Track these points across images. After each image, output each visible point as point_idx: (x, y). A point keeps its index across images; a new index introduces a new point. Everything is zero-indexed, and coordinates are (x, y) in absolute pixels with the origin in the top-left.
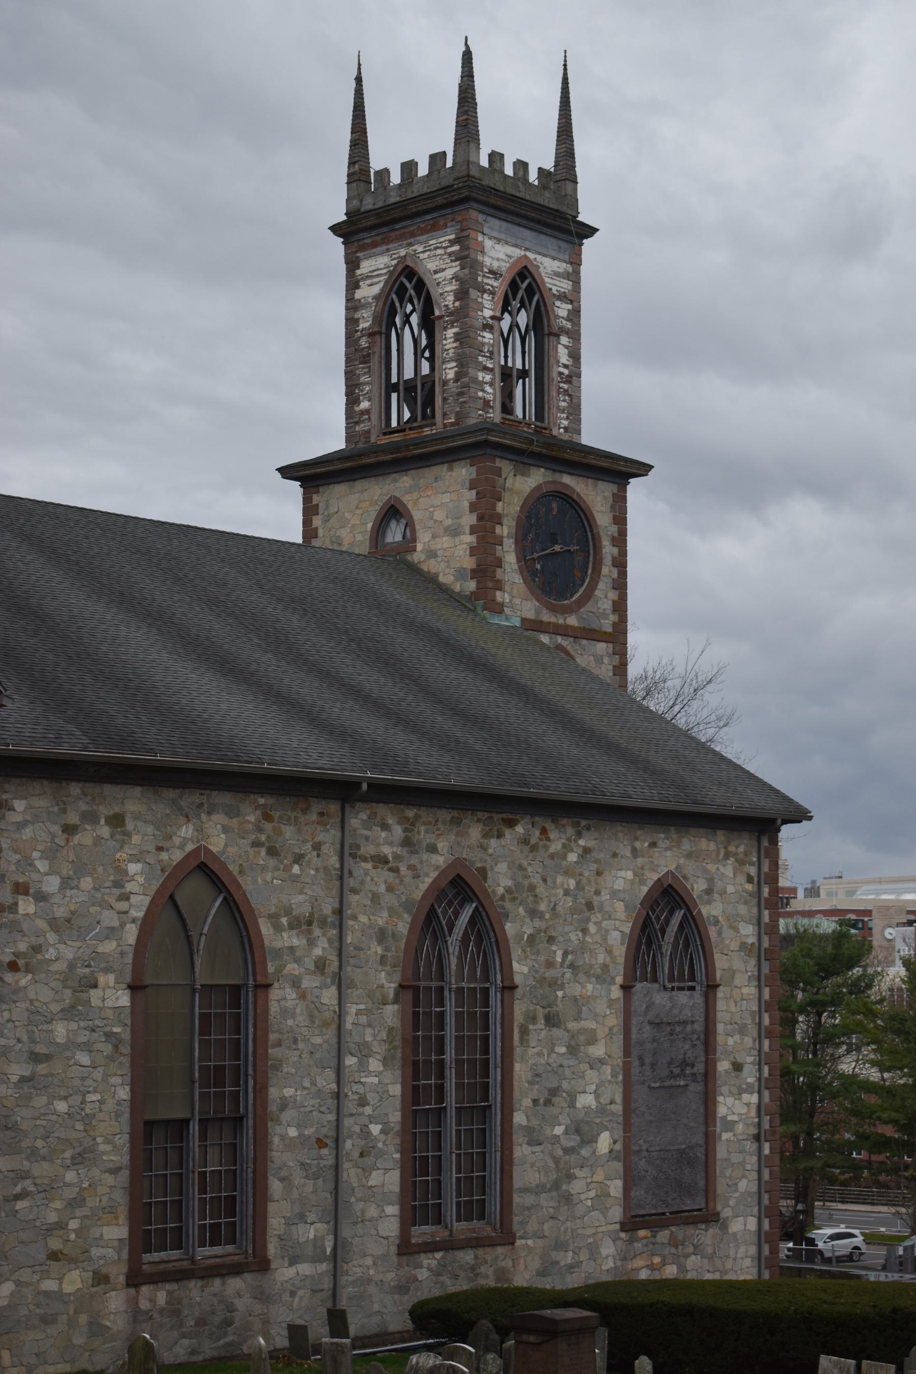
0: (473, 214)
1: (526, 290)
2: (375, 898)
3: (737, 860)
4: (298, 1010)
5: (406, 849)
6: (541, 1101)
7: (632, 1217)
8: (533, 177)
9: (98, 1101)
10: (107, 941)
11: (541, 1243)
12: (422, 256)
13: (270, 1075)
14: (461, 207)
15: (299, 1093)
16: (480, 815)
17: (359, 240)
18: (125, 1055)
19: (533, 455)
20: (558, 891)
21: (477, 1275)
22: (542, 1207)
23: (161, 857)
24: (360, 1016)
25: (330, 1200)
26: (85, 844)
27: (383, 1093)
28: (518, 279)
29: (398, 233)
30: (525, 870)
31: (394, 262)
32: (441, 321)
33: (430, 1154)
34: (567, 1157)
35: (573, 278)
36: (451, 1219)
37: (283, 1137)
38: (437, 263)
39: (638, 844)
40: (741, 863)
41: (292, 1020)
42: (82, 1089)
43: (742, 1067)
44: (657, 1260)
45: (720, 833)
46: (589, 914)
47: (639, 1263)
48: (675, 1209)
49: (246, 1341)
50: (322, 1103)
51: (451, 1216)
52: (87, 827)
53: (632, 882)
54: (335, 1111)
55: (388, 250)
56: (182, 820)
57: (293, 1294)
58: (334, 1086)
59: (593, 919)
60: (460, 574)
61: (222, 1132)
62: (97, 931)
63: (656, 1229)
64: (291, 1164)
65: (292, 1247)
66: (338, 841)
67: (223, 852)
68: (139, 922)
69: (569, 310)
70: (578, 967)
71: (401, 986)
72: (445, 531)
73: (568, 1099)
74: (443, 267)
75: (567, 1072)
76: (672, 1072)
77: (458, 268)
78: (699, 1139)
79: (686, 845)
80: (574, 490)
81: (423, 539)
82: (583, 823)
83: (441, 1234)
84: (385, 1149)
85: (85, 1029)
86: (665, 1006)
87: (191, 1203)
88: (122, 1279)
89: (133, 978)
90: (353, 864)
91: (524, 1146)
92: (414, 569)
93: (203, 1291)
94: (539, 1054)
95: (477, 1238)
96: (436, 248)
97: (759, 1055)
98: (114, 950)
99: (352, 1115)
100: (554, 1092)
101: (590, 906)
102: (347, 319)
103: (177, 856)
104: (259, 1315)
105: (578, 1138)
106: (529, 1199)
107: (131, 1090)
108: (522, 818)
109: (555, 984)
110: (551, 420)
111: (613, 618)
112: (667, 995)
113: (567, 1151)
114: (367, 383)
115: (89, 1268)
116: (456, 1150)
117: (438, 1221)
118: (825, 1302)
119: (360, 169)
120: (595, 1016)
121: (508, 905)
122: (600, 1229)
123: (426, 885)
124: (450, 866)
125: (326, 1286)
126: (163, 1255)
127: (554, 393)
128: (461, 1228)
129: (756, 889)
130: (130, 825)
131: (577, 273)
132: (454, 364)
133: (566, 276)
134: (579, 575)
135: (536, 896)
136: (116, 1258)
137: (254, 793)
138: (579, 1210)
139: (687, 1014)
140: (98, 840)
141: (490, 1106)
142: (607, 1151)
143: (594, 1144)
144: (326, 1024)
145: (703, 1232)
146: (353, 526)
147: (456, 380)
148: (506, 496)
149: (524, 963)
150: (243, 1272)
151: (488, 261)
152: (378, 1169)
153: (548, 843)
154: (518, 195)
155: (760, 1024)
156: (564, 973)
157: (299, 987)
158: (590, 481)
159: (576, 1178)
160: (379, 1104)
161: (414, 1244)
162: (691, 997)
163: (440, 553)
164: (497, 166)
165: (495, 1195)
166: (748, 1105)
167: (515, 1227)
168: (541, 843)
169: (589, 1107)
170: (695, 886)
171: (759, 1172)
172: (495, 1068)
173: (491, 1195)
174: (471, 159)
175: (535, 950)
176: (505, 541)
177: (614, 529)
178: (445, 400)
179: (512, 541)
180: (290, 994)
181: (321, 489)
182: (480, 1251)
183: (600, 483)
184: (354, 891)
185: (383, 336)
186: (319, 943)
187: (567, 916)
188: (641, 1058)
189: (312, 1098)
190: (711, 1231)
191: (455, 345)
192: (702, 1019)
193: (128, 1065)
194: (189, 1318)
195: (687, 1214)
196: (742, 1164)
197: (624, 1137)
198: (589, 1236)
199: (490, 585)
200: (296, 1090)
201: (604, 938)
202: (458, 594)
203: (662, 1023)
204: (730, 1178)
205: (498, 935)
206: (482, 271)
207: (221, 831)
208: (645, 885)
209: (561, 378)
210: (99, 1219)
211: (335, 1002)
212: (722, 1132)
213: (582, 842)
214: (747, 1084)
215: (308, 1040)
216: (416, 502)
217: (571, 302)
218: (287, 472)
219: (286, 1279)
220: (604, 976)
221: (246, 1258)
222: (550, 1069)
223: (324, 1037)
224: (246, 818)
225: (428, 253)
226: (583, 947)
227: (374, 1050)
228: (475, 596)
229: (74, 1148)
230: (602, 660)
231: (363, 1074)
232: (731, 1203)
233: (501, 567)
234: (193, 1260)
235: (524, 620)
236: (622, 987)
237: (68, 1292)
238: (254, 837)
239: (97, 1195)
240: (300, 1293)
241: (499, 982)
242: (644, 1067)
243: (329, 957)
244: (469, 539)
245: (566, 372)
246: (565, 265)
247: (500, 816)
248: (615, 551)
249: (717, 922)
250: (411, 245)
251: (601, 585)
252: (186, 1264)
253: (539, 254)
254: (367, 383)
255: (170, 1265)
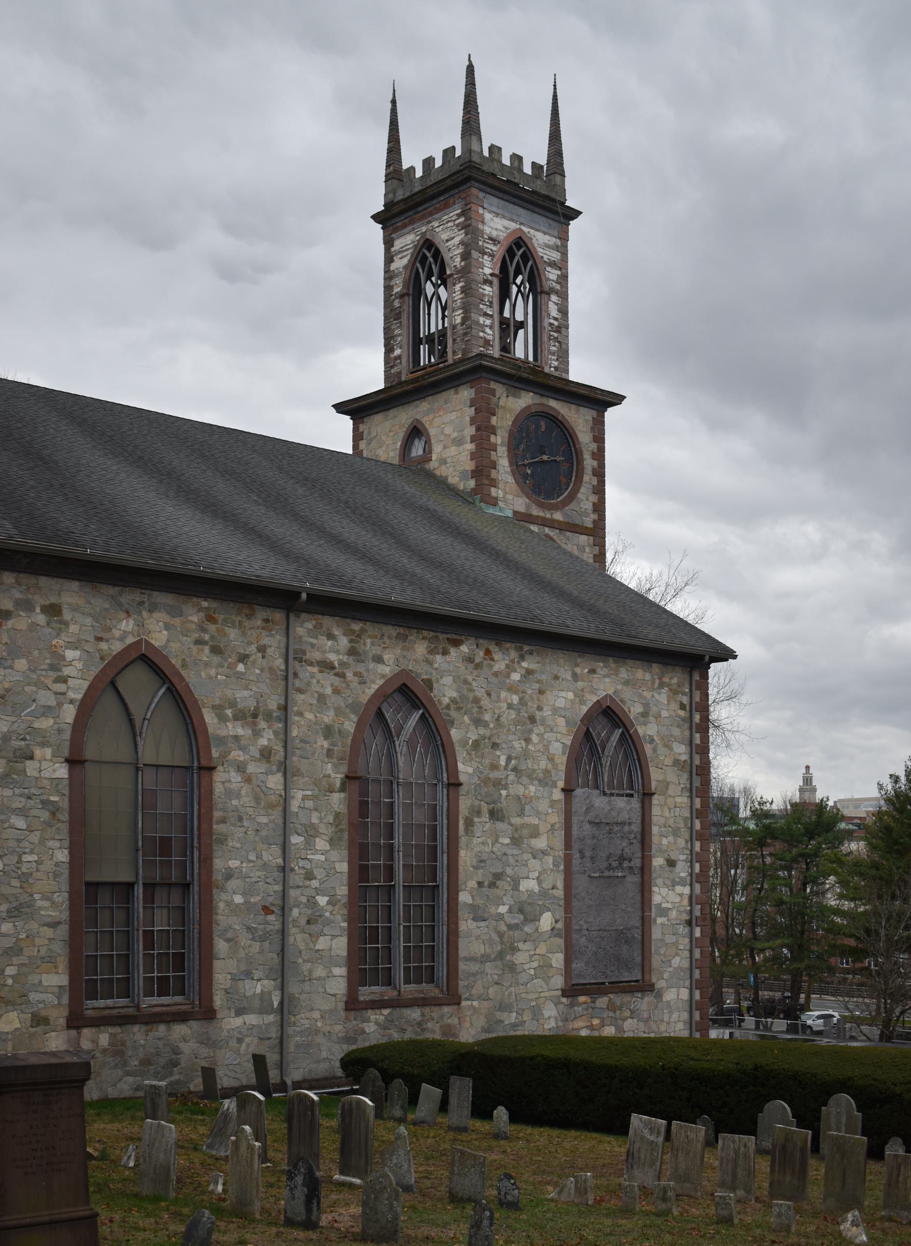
0: (474, 191)
1: (521, 256)
2: (322, 698)
3: (670, 690)
4: (243, 792)
5: (351, 658)
6: (486, 883)
7: (573, 985)
8: (527, 169)
9: (35, 861)
10: (43, 718)
11: (485, 1004)
12: (437, 230)
13: (214, 848)
14: (465, 187)
15: (244, 865)
16: (425, 633)
17: (393, 225)
18: (63, 822)
19: (521, 380)
20: (502, 704)
21: (423, 1030)
22: (487, 974)
23: (100, 647)
24: (306, 801)
25: (276, 960)
26: (19, 628)
27: (330, 869)
28: (514, 247)
29: (420, 214)
30: (470, 684)
31: (419, 237)
32: (451, 279)
33: (380, 925)
34: (511, 932)
35: (562, 250)
36: (400, 982)
37: (229, 903)
38: (448, 233)
39: (578, 670)
40: (675, 692)
41: (237, 801)
42: (17, 849)
43: (675, 864)
44: (596, 1022)
45: (655, 666)
46: (531, 726)
47: (579, 1024)
48: (612, 980)
49: (193, 1080)
50: (268, 875)
51: (399, 979)
52: (21, 613)
53: (572, 702)
54: (281, 883)
55: (414, 229)
56: (123, 615)
57: (240, 1041)
58: (280, 861)
59: (536, 730)
60: (463, 475)
61: (169, 898)
62: (33, 708)
63: (595, 996)
64: (237, 927)
65: (238, 1000)
66: (283, 645)
67: (165, 647)
68: (77, 703)
69: (558, 275)
70: (522, 770)
71: (347, 777)
72: (452, 443)
73: (512, 883)
74: (453, 236)
75: (511, 860)
76: (610, 865)
77: (464, 235)
78: (636, 922)
79: (624, 674)
80: (559, 412)
81: (437, 450)
82: (526, 648)
83: (389, 993)
84: (332, 917)
85: (21, 796)
86: (603, 809)
87: (136, 957)
88: (62, 1021)
89: (71, 753)
90: (298, 667)
91: (470, 921)
92: (430, 475)
93: (147, 1035)
94: (483, 843)
95: (423, 998)
96: (447, 222)
97: (691, 854)
98: (51, 726)
99: (298, 887)
100: (498, 876)
101: (532, 720)
102: (385, 287)
103: (117, 647)
104: (205, 1058)
105: (522, 917)
106: (474, 967)
107: (70, 853)
108: (467, 639)
109: (498, 784)
110: (543, 360)
111: (594, 517)
112: (606, 799)
113: (510, 927)
114: (399, 335)
115: (27, 1011)
116: (404, 922)
117: (389, 982)
118: (692, 1059)
119: (394, 170)
120: (538, 813)
121: (453, 713)
122: (542, 995)
123: (373, 691)
124: (396, 676)
125: (274, 1035)
126: (110, 1002)
127: (545, 339)
128: (410, 990)
129: (688, 715)
130: (67, 615)
131: (565, 246)
132: (461, 311)
133: (556, 248)
134: (564, 480)
135: (480, 707)
136: (56, 1002)
137: (197, 597)
138: (523, 978)
139: (625, 816)
140: (34, 626)
141: (438, 886)
142: (549, 928)
143: (537, 923)
144: (271, 806)
145: (639, 999)
146: (387, 445)
147: (462, 324)
148: (499, 412)
149: (468, 764)
150: (188, 1020)
151: (487, 230)
152: (325, 935)
153: (492, 663)
154: (514, 180)
155: (691, 828)
156: (508, 775)
157: (244, 772)
158: (573, 406)
159: (520, 950)
160: (325, 879)
161: (362, 1001)
162: (629, 802)
163: (449, 460)
164: (496, 156)
165: (443, 962)
166: (681, 895)
167: (461, 990)
168: (485, 662)
169: (532, 891)
170: (632, 709)
171: (691, 951)
172: (443, 853)
173: (439, 962)
174: (472, 148)
175: (480, 754)
176: (499, 448)
178: (454, 340)
179: (505, 448)
180: (235, 777)
181: (365, 420)
182: (427, 1010)
183: (582, 408)
184: (300, 691)
185: (411, 297)
186: (264, 734)
187: (511, 727)
188: (581, 852)
189: (259, 870)
190: (646, 999)
191: (461, 296)
192: (639, 822)
193: (66, 831)
194: (134, 1058)
195: (625, 984)
196: (676, 944)
197: (565, 917)
198: (532, 1000)
199: (486, 482)
200: (242, 862)
201: (547, 748)
202: (462, 491)
203: (601, 823)
204: (665, 955)
205: (444, 739)
206: (483, 237)
207: (163, 628)
208: (585, 705)
209: (552, 328)
210: (38, 967)
211: (281, 787)
212: (657, 916)
213: (525, 664)
214: (680, 878)
215: (254, 819)
216: (431, 422)
217: (560, 269)
218: (341, 408)
219: (233, 1027)
220: (546, 780)
221: (193, 1008)
222: (495, 856)
223: (270, 817)
224: (189, 618)
225: (442, 227)
226: (526, 754)
227: (321, 831)
228: (474, 491)
229: (10, 902)
230: (584, 549)
231: (309, 852)
232: (665, 976)
233: (495, 469)
234: (138, 1007)
235: (515, 513)
236: (563, 790)
237: (6, 1031)
238: (197, 635)
239: (34, 946)
240: (247, 1040)
241: (445, 779)
242: (584, 859)
243: (275, 747)
244: (470, 447)
245: (556, 323)
246: (554, 239)
247: (445, 636)
248: (595, 463)
249: (652, 740)
250: (430, 222)
251: (583, 490)
252: (131, 1011)
253: (533, 228)
254: (399, 335)
255: (115, 1012)
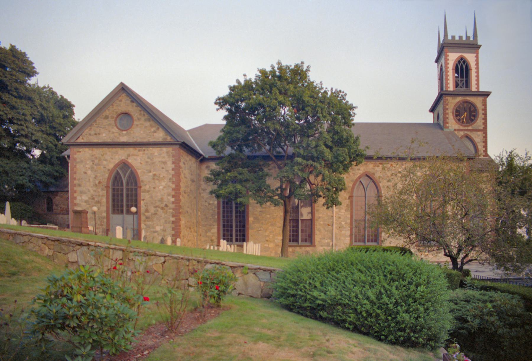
177: (483, 107)
